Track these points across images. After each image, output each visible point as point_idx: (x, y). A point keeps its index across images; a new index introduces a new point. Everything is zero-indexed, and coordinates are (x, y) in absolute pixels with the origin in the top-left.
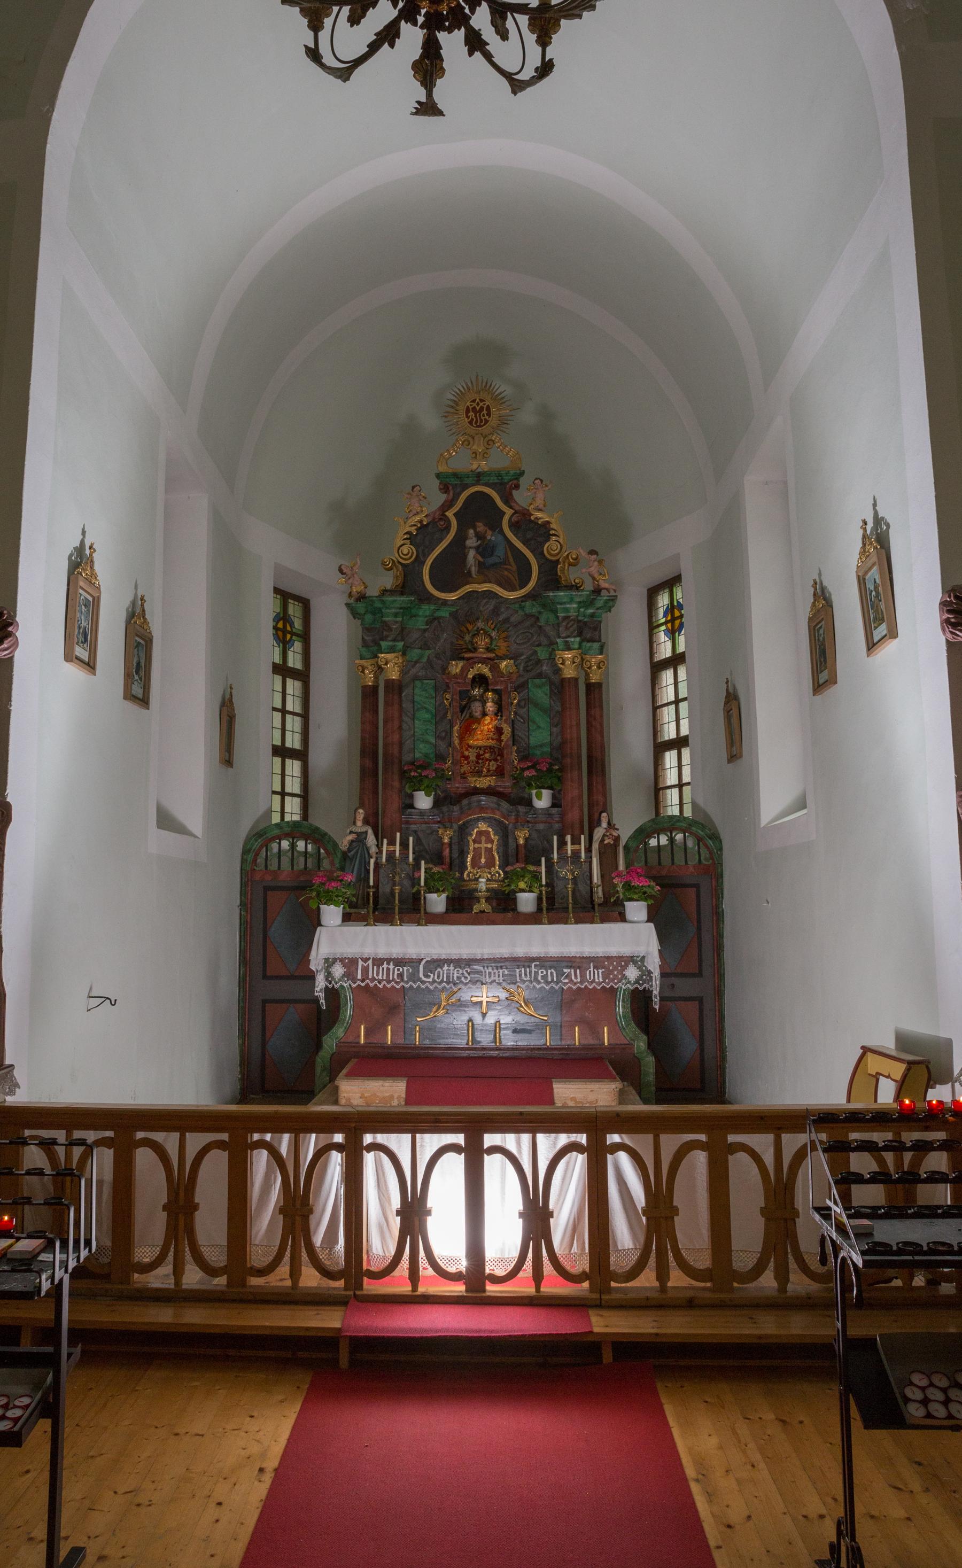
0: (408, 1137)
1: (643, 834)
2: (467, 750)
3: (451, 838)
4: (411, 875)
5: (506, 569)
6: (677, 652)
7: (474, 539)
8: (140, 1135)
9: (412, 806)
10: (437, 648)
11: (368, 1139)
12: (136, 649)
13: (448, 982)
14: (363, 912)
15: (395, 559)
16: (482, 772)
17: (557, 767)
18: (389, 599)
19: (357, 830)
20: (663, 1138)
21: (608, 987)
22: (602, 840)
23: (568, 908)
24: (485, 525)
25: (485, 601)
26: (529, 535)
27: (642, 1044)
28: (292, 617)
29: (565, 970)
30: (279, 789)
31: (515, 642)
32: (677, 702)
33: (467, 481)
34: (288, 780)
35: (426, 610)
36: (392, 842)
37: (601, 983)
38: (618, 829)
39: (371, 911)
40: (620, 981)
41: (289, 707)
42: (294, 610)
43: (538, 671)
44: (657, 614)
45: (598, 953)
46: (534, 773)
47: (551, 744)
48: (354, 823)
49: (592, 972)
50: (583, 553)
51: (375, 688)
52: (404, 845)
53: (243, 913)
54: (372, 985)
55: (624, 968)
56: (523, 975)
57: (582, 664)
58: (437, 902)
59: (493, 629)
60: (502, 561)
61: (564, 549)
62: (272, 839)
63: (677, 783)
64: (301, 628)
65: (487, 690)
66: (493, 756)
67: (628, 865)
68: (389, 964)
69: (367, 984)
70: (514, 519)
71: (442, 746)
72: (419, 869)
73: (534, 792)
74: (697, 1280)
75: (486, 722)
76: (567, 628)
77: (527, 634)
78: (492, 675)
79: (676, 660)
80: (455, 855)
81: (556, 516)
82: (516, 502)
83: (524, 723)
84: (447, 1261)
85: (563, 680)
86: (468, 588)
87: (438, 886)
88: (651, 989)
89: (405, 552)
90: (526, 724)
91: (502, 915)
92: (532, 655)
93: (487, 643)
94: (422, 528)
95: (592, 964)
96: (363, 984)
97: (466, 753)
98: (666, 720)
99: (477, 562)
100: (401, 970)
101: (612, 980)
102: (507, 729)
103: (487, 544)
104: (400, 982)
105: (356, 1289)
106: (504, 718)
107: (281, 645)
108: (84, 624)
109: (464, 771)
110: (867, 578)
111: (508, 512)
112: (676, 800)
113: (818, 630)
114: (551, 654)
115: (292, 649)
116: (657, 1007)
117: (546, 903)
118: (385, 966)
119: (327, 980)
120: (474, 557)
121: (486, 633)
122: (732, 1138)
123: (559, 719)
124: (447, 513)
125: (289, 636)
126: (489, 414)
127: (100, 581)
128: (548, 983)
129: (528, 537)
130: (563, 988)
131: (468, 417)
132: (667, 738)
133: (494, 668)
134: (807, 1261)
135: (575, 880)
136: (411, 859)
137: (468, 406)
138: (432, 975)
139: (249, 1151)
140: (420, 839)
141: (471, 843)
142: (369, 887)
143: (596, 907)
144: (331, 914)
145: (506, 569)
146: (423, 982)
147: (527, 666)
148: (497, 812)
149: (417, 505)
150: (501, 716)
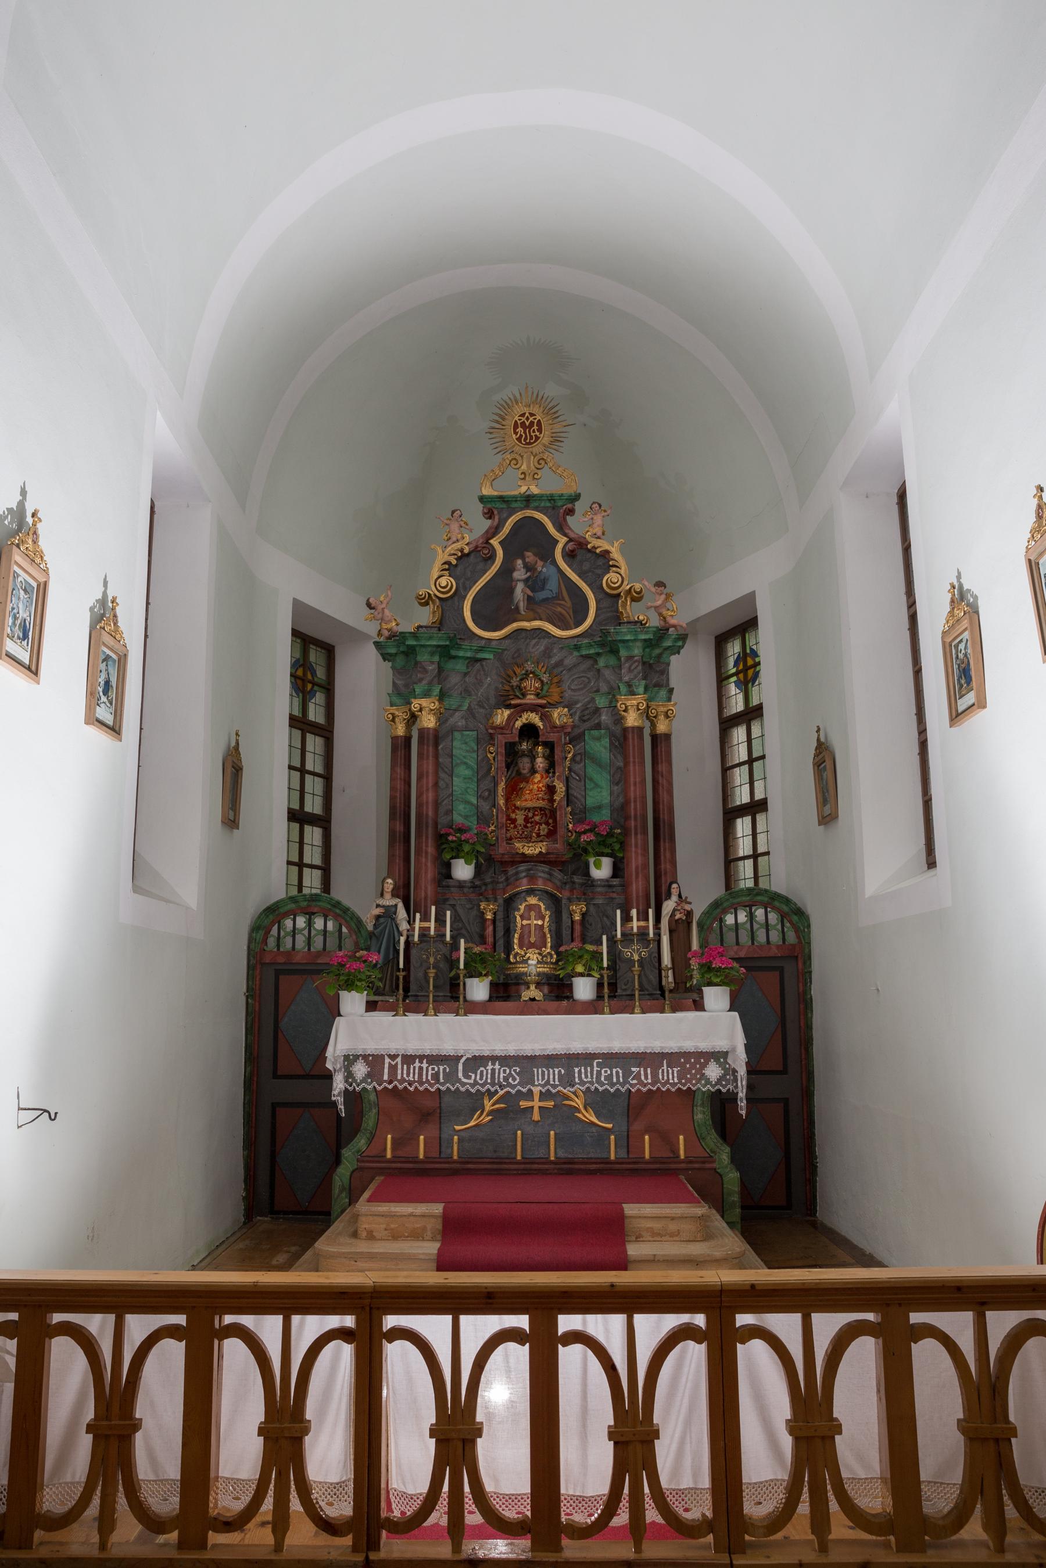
0: (448, 1319)
1: (717, 909)
2: (514, 812)
3: (495, 913)
4: (449, 957)
5: (560, 605)
6: (751, 706)
7: (523, 571)
8: (57, 1318)
9: (449, 876)
10: (479, 694)
11: (391, 1321)
12: (105, 663)
13: (493, 1084)
14: (391, 1000)
15: (431, 593)
16: (531, 838)
17: (619, 831)
19: (384, 903)
20: (816, 1318)
21: (685, 1088)
22: (673, 915)
23: (634, 995)
24: (535, 555)
25: (534, 641)
26: (586, 566)
27: (725, 1157)
28: (314, 665)
29: (633, 1069)
30: (296, 859)
31: (569, 688)
33: (514, 505)
34: (307, 849)
36: (425, 918)
37: (676, 1084)
38: (690, 903)
39: (401, 999)
40: (699, 1081)
41: (309, 766)
42: (315, 656)
43: (596, 722)
44: (726, 664)
45: (629, 1048)
46: (592, 838)
47: (611, 806)
48: (382, 895)
49: (665, 1071)
50: (649, 585)
51: (408, 739)
52: (440, 921)
53: (250, 1001)
54: (400, 1087)
55: (704, 1066)
56: (583, 1076)
57: (647, 714)
58: (478, 990)
59: (545, 673)
60: (555, 595)
61: (625, 583)
62: (286, 915)
63: (751, 853)
64: (324, 678)
65: (537, 744)
66: (544, 818)
67: (704, 944)
68: (421, 1062)
69: (396, 1086)
70: (571, 546)
71: (485, 806)
72: (458, 949)
73: (592, 860)
74: (871, 1533)
75: (536, 781)
76: (630, 670)
77: (583, 679)
78: (543, 725)
80: (500, 933)
81: (616, 544)
82: (570, 529)
83: (580, 781)
84: (504, 1500)
85: (625, 730)
86: (515, 625)
87: (480, 969)
88: (735, 1091)
89: (444, 584)
90: (583, 782)
91: (556, 1004)
92: (589, 702)
93: (537, 689)
94: (463, 557)
95: (665, 1062)
96: (390, 1087)
97: (513, 816)
98: (737, 782)
99: (526, 597)
100: (436, 1069)
101: (689, 1081)
102: (560, 787)
103: (537, 576)
104: (435, 1084)
105: (369, 1549)
106: (557, 774)
107: (301, 695)
108: (23, 614)
109: (511, 836)
110: (1041, 562)
111: (562, 540)
112: (750, 873)
113: (957, 646)
114: (611, 702)
115: (313, 701)
116: (743, 1113)
117: (609, 989)
118: (417, 1064)
119: (346, 1081)
120: (522, 591)
121: (536, 676)
122: (916, 1318)
123: (620, 777)
124: (491, 541)
125: (309, 686)
126: (540, 430)
127: (47, 562)
128: (612, 1085)
129: (584, 568)
130: (630, 1090)
131: (516, 433)
132: (738, 803)
133: (544, 717)
134: (1031, 1502)
135: (641, 962)
136: (448, 938)
137: (516, 421)
138: (473, 1076)
139: (216, 1342)
140: (459, 915)
141: (518, 918)
142: (398, 970)
143: (667, 993)
144: (353, 1002)
145: (560, 605)
146: (464, 1084)
147: (584, 716)
148: (550, 884)
149: (457, 531)
150: (554, 773)
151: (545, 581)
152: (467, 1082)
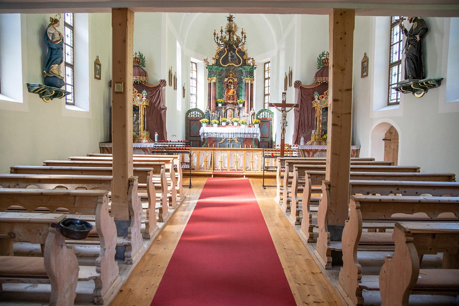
18: (214, 67)
32: (269, 87)
35: (221, 68)
62: (191, 112)
70: (238, 51)
79: (269, 78)
86: (229, 64)
151: (234, 57)
152: (222, 136)
